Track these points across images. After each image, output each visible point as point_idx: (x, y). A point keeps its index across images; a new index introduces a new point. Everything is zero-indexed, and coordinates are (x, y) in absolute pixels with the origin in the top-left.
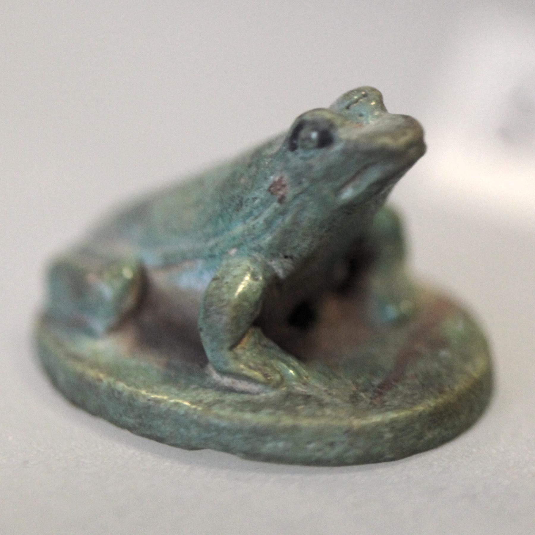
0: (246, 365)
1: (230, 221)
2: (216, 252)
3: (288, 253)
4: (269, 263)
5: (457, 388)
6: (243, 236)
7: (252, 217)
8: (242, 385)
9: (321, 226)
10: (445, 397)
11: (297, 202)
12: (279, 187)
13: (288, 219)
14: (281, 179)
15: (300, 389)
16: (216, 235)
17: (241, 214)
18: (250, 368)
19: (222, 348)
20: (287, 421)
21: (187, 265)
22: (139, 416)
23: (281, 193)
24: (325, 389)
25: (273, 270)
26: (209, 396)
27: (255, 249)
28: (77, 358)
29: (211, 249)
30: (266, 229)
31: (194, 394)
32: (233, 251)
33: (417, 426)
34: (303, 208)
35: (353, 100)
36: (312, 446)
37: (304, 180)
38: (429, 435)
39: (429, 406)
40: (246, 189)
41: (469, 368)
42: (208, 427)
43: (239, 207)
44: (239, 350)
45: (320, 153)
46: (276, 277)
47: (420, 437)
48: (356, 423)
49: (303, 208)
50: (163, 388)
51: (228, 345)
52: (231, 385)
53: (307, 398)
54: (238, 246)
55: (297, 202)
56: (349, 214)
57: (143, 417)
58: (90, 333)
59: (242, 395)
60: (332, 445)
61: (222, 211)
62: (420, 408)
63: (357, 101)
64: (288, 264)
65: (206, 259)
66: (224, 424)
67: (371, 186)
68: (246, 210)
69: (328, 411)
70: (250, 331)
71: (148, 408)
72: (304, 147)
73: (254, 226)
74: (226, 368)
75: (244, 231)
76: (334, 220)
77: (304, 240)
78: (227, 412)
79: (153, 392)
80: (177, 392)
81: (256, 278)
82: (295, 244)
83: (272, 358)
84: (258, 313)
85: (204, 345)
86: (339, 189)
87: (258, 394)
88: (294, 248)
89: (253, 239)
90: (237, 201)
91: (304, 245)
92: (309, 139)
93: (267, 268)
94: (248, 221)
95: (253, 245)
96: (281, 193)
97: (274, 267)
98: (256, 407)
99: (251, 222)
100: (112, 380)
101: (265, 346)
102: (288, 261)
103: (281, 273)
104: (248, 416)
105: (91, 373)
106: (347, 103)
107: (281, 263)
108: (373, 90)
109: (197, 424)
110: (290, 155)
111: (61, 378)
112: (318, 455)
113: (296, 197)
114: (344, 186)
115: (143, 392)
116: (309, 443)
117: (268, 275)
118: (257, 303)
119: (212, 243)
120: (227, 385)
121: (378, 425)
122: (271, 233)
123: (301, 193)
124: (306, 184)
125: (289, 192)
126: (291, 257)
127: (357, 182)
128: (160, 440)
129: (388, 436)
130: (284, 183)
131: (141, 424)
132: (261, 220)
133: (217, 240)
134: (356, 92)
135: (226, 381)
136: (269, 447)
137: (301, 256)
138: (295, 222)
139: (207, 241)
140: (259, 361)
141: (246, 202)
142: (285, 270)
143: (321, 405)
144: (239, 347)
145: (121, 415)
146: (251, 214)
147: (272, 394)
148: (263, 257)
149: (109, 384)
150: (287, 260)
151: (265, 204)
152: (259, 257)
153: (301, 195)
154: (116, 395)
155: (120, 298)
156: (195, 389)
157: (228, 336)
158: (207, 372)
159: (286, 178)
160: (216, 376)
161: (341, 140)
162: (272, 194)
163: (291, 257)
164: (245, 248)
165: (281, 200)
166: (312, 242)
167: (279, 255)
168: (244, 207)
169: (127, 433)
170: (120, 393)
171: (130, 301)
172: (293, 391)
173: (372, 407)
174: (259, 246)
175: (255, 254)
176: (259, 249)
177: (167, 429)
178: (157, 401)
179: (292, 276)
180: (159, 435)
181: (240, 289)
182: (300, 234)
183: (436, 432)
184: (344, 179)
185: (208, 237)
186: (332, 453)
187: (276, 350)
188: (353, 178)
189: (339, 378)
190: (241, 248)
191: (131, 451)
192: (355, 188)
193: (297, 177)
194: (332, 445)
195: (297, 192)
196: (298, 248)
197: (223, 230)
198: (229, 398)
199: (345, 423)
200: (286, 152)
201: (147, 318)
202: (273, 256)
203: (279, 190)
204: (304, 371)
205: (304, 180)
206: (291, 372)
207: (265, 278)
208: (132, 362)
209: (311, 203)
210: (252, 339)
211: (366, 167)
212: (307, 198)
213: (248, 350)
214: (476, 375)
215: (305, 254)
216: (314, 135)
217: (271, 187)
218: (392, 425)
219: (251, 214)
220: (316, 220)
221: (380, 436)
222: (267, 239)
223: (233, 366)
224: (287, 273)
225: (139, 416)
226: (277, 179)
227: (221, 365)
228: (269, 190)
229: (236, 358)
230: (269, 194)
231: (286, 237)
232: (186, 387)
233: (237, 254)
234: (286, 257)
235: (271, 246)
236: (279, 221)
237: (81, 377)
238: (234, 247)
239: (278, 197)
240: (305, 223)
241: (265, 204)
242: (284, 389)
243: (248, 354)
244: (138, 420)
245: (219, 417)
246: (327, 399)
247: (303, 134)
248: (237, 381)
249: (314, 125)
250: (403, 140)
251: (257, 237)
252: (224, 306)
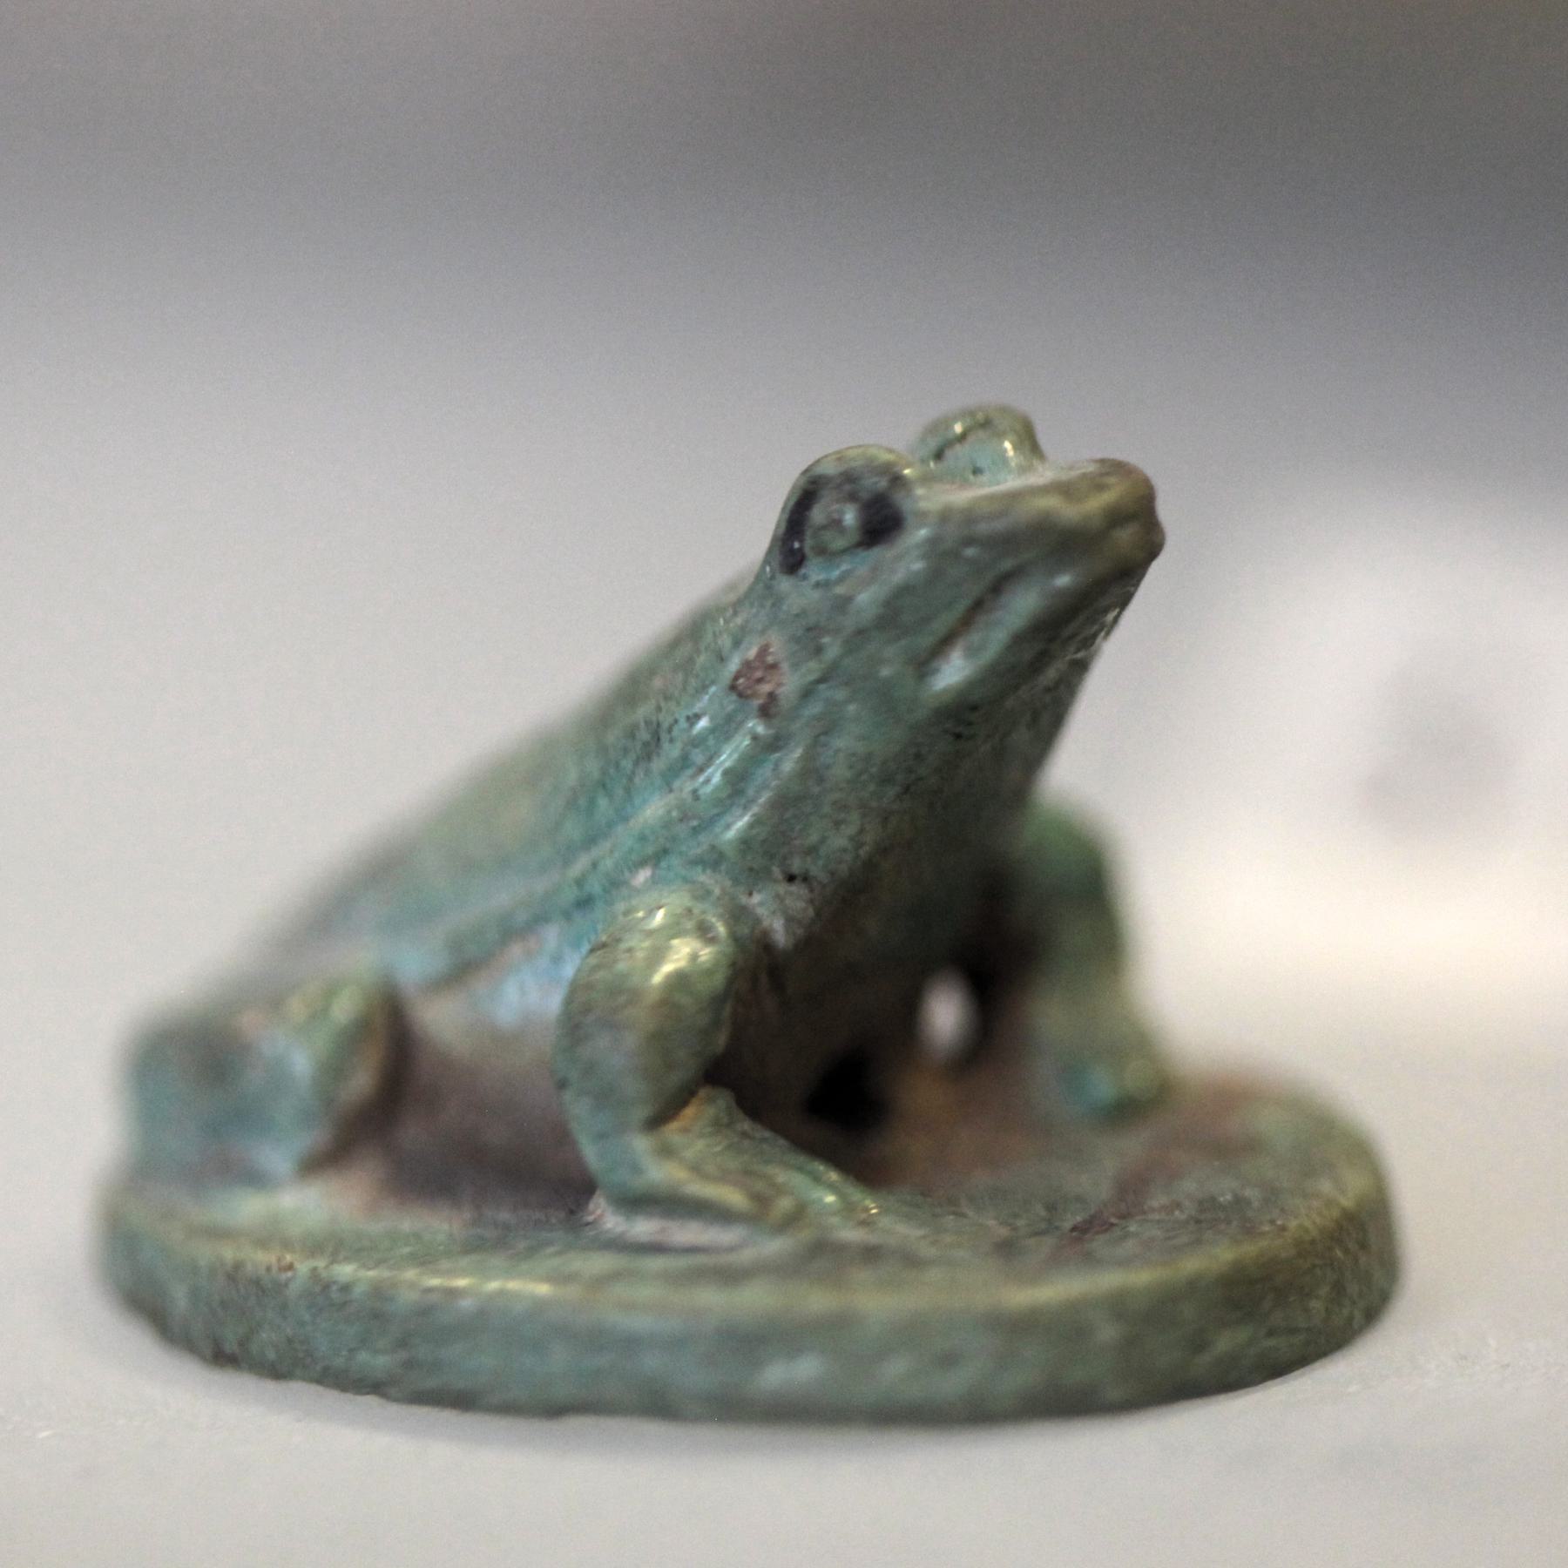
2: (595, 886)
3: (796, 865)
4: (744, 900)
6: (667, 824)
7: (690, 772)
8: (688, 1233)
9: (886, 779)
10: (1264, 1243)
11: (814, 708)
12: (758, 674)
13: (790, 761)
14: (764, 651)
15: (851, 1234)
16: (590, 841)
17: (658, 765)
20: (817, 1301)
21: (516, 950)
23: (766, 688)
25: (758, 921)
26: (600, 1263)
27: (699, 862)
29: (580, 882)
30: (730, 796)
31: (556, 1262)
32: (643, 875)
34: (828, 726)
35: (950, 436)
37: (826, 640)
38: (1225, 1342)
40: (667, 698)
41: (1326, 1186)
42: (595, 1339)
43: (651, 748)
46: (765, 944)
47: (1198, 1344)
49: (828, 726)
50: (464, 1262)
51: (641, 1113)
53: (871, 1254)
54: (657, 858)
55: (814, 708)
56: (958, 736)
58: (255, 1179)
61: (604, 772)
63: (962, 438)
64: (798, 899)
65: (567, 916)
66: (641, 1323)
67: (1018, 640)
68: (672, 751)
71: (425, 1311)
72: (822, 551)
73: (695, 792)
74: (638, 1184)
75: (669, 812)
76: (918, 757)
77: (837, 824)
79: (437, 1273)
81: (710, 935)
82: (814, 838)
83: (767, 1162)
84: (721, 1040)
85: (574, 1126)
87: (731, 1249)
88: (812, 851)
89: (696, 831)
90: (644, 735)
91: (839, 841)
92: (836, 524)
93: (737, 914)
94: (677, 784)
96: (766, 688)
98: (730, 1276)
99: (684, 786)
101: (744, 1135)
102: (797, 889)
103: (780, 933)
105: (260, 1259)
106: (933, 444)
107: (777, 896)
108: (1005, 410)
110: (785, 584)
111: (179, 1297)
113: (807, 693)
114: (945, 643)
117: (744, 930)
118: (718, 1001)
119: (581, 864)
123: (822, 680)
125: (789, 684)
126: (806, 879)
127: (975, 637)
130: (770, 659)
131: (409, 1364)
132: (715, 775)
133: (595, 852)
135: (644, 1228)
137: (833, 874)
138: (811, 770)
139: (567, 863)
140: (733, 1163)
141: (670, 730)
142: (790, 920)
143: (911, 1261)
144: (674, 1125)
146: (684, 761)
147: (774, 1246)
148: (728, 883)
150: (793, 888)
151: (725, 728)
152: (713, 881)
153: (822, 687)
154: (335, 1295)
155: (334, 1069)
156: (559, 1253)
159: (778, 645)
161: (922, 516)
163: (806, 879)
164: (675, 861)
165: (766, 711)
166: (862, 831)
167: (768, 872)
168: (666, 745)
169: (372, 1401)
170: (346, 1288)
171: (361, 1082)
173: (1056, 1262)
174: (713, 847)
175: (704, 877)
176: (714, 859)
178: (452, 1293)
179: (810, 944)
181: (668, 968)
184: (941, 624)
185: (567, 855)
186: (953, 1384)
188: (966, 622)
190: (663, 864)
192: (971, 652)
193: (809, 638)
195: (812, 677)
196: (823, 851)
197: (610, 825)
198: (656, 1263)
200: (773, 577)
201: (413, 1133)
202: (754, 877)
203: (760, 681)
204: (856, 1194)
205: (826, 640)
207: (735, 938)
208: (376, 1227)
209: (852, 708)
210: (710, 1111)
211: (997, 587)
212: (840, 694)
214: (1347, 1202)
215: (843, 869)
216: (850, 517)
217: (736, 678)
218: (1117, 1305)
219: (684, 761)
220: (868, 757)
222: (738, 824)
223: (661, 1173)
224: (800, 932)
225: (402, 1343)
226: (752, 653)
228: (733, 688)
229: (666, 1152)
230: (734, 697)
231: (788, 815)
232: (532, 1251)
233: (654, 881)
234: (791, 878)
236: (765, 772)
237: (234, 1274)
238: (642, 863)
239: (757, 702)
240: (840, 772)
241: (725, 728)
244: (402, 1355)
247: (817, 515)
249: (847, 484)
250: (1095, 505)
251: (707, 824)
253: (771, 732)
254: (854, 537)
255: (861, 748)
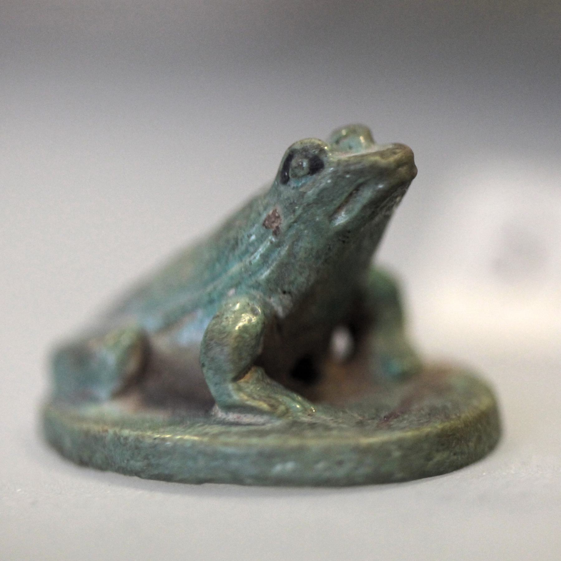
0: (250, 396)
1: (227, 263)
2: (215, 295)
3: (286, 288)
4: (267, 300)
5: (463, 416)
6: (240, 273)
8: (247, 418)
9: (318, 257)
11: (293, 232)
12: (273, 219)
13: (284, 250)
14: (275, 211)
15: (306, 419)
17: (237, 252)
18: (254, 398)
19: (225, 380)
20: (294, 442)
22: (146, 457)
23: (275, 225)
24: (331, 418)
25: (272, 307)
26: (216, 429)
28: (82, 419)
29: (210, 294)
31: (200, 429)
32: (232, 292)
33: (426, 446)
34: (298, 238)
36: (321, 466)
38: (438, 457)
39: (436, 427)
42: (213, 456)
44: (242, 382)
45: (310, 180)
46: (275, 316)
47: (429, 458)
48: (365, 441)
49: (298, 238)
51: (231, 376)
52: (237, 420)
53: (312, 426)
54: (237, 285)
55: (293, 232)
57: (150, 457)
59: (247, 427)
60: (340, 463)
62: (427, 429)
64: (287, 300)
66: (230, 450)
67: (365, 207)
69: (335, 433)
70: (253, 369)
71: (154, 446)
72: (295, 176)
74: (229, 401)
77: (301, 274)
78: (233, 439)
80: (183, 430)
82: (292, 278)
83: (276, 393)
84: (260, 350)
86: (333, 213)
87: (263, 424)
88: (291, 283)
89: (250, 276)
91: (301, 279)
93: (265, 305)
95: (252, 281)
96: (275, 225)
97: (274, 304)
98: (262, 434)
100: (117, 430)
101: (268, 384)
103: (280, 311)
104: (254, 441)
109: (204, 454)
110: (282, 188)
111: (68, 443)
112: (327, 474)
113: (290, 227)
115: (149, 433)
116: (317, 462)
117: (268, 311)
119: (210, 288)
120: (232, 420)
121: (384, 444)
122: (268, 268)
123: (295, 222)
124: (299, 212)
125: (283, 223)
126: (290, 293)
127: (350, 206)
128: (168, 478)
129: (397, 454)
131: (149, 465)
132: (257, 256)
134: (354, 192)
135: (232, 417)
136: (278, 469)
138: (291, 254)
142: (284, 307)
143: (327, 428)
144: (242, 380)
145: (128, 460)
146: (246, 251)
147: (278, 423)
148: (262, 294)
149: (115, 434)
150: (286, 296)
151: (261, 239)
152: (258, 294)
153: (295, 224)
155: (122, 362)
157: (231, 366)
158: (213, 413)
159: (279, 209)
160: (220, 414)
161: (330, 163)
162: (266, 227)
164: (244, 287)
165: (275, 233)
166: (310, 275)
167: (276, 290)
170: (126, 438)
171: (132, 365)
172: (299, 420)
174: (256, 282)
175: (253, 292)
177: (174, 465)
179: (292, 316)
180: (167, 472)
182: (297, 267)
183: (445, 455)
184: (337, 203)
186: (341, 472)
187: (280, 388)
188: (347, 201)
189: (344, 412)
191: (140, 492)
192: (348, 212)
193: (290, 207)
194: (340, 463)
195: (292, 221)
198: (235, 429)
199: (352, 442)
203: (273, 222)
204: (307, 405)
206: (298, 406)
210: (256, 375)
211: (357, 189)
212: (302, 227)
213: (252, 384)
217: (265, 221)
218: (400, 444)
220: (312, 249)
221: (388, 454)
222: (266, 273)
223: (238, 397)
225: (146, 457)
226: (271, 212)
227: (225, 398)
228: (264, 225)
229: (240, 389)
230: (264, 228)
232: (192, 425)
234: (284, 292)
235: (268, 280)
236: (275, 255)
237: (87, 433)
238: (231, 287)
239: (272, 230)
240: (302, 254)
241: (261, 239)
242: (290, 418)
243: (252, 387)
244: (146, 462)
245: (226, 444)
246: (333, 425)
247: (294, 163)
248: (242, 416)
249: (304, 151)
251: (254, 273)
252: (223, 338)
253: (277, 240)
254: (306, 170)
255: (309, 246)
